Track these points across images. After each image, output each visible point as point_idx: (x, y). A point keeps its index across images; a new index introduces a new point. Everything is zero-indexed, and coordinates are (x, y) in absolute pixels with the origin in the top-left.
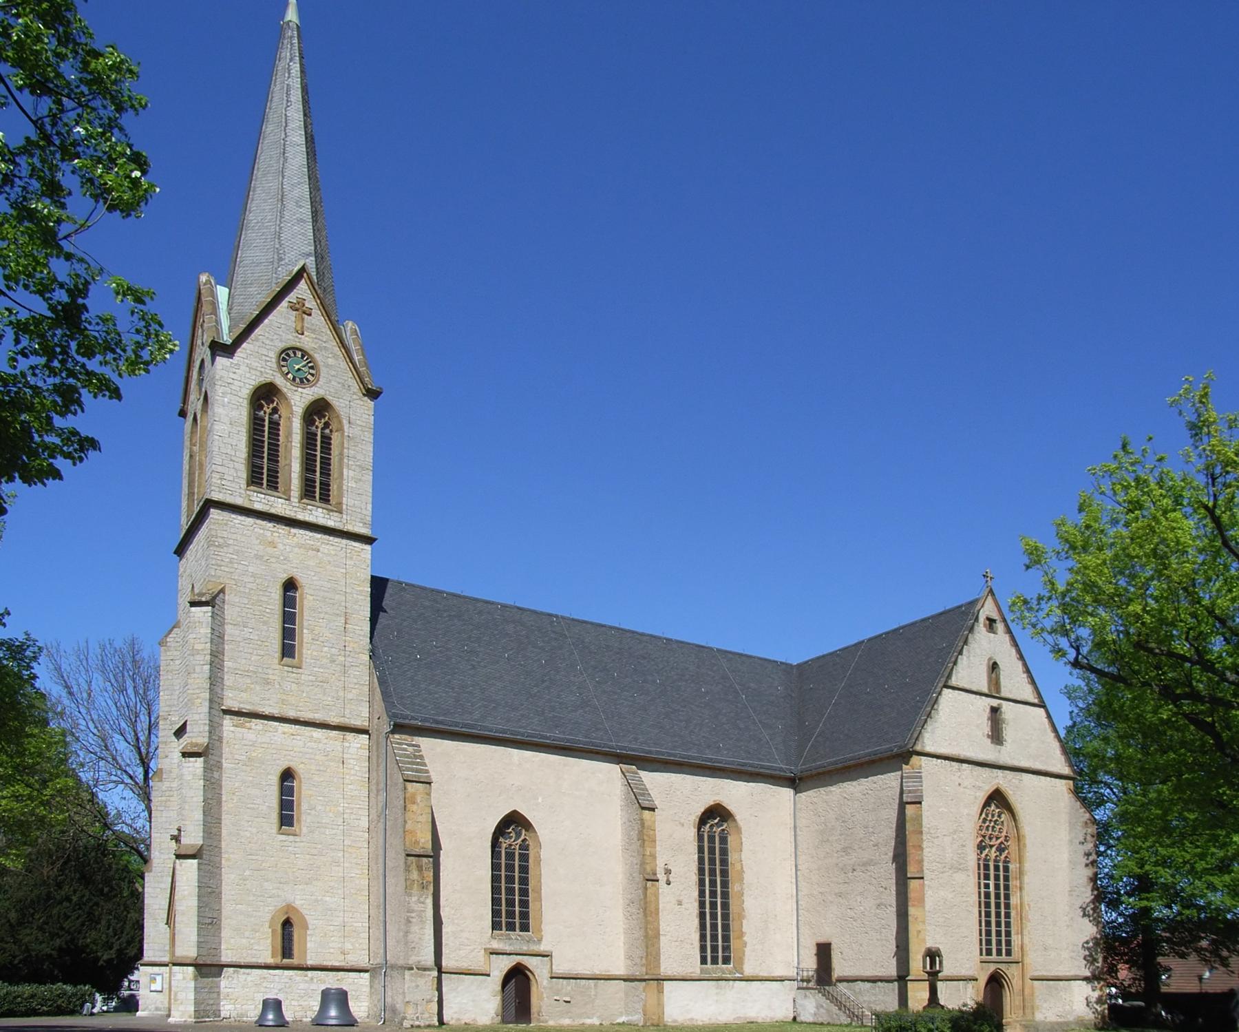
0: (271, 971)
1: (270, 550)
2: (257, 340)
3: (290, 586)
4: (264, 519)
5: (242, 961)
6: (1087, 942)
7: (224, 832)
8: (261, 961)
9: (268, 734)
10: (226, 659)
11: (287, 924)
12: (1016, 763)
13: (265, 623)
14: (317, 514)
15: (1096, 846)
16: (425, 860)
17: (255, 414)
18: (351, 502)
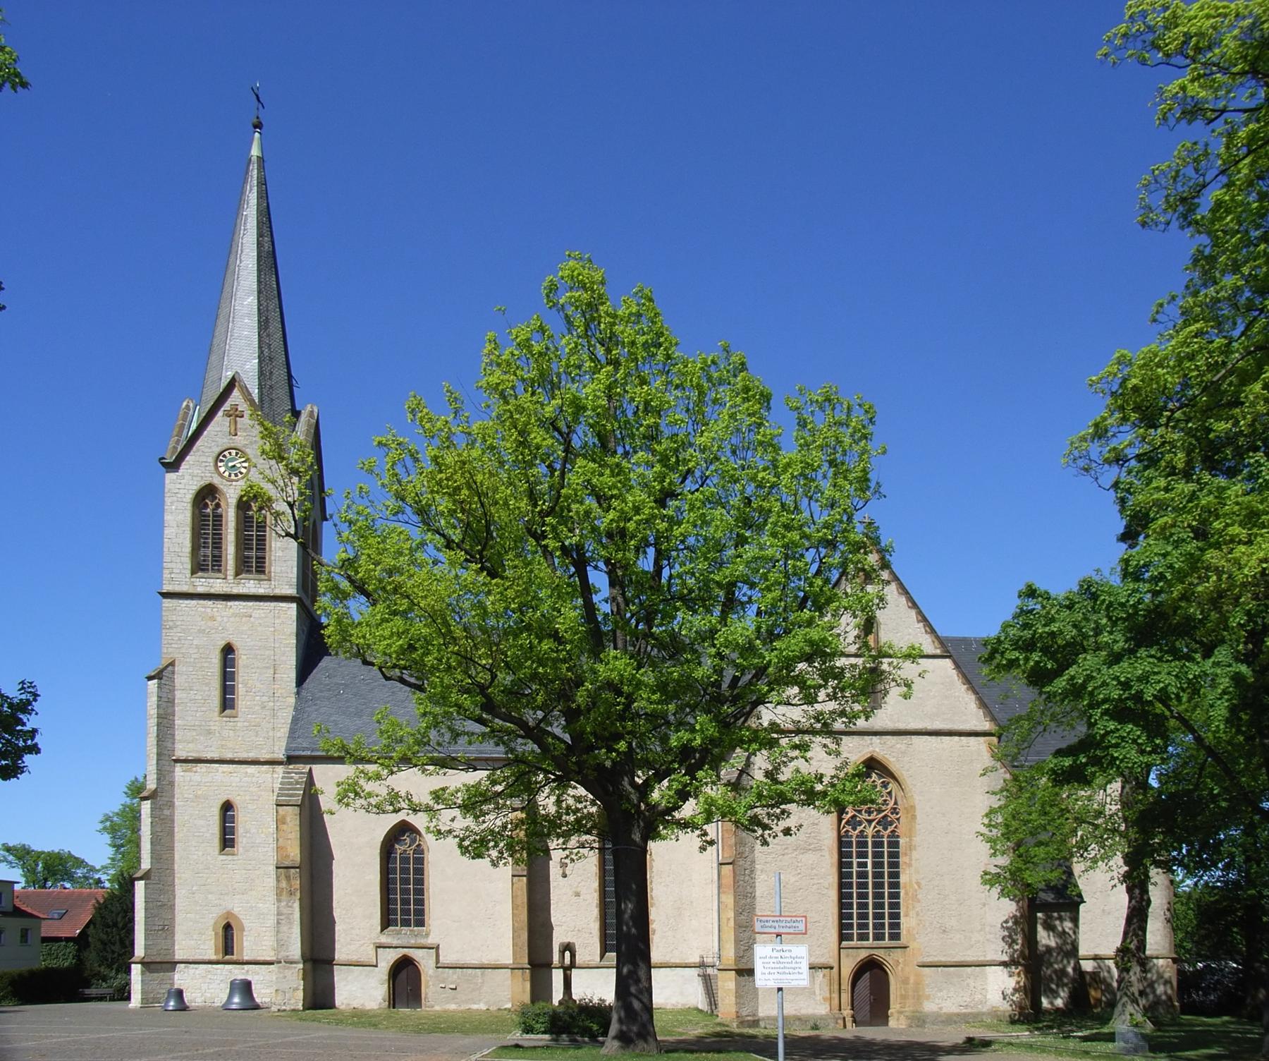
0: (214, 966)
1: (210, 624)
2: (198, 450)
3: (228, 650)
4: (204, 599)
5: (191, 958)
6: (1006, 922)
7: (177, 857)
8: (206, 958)
9: (211, 774)
10: (176, 718)
11: (228, 928)
12: (901, 726)
13: (207, 685)
14: (250, 586)
15: (686, 825)
16: (293, 870)
17: (201, 512)
18: (278, 569)
